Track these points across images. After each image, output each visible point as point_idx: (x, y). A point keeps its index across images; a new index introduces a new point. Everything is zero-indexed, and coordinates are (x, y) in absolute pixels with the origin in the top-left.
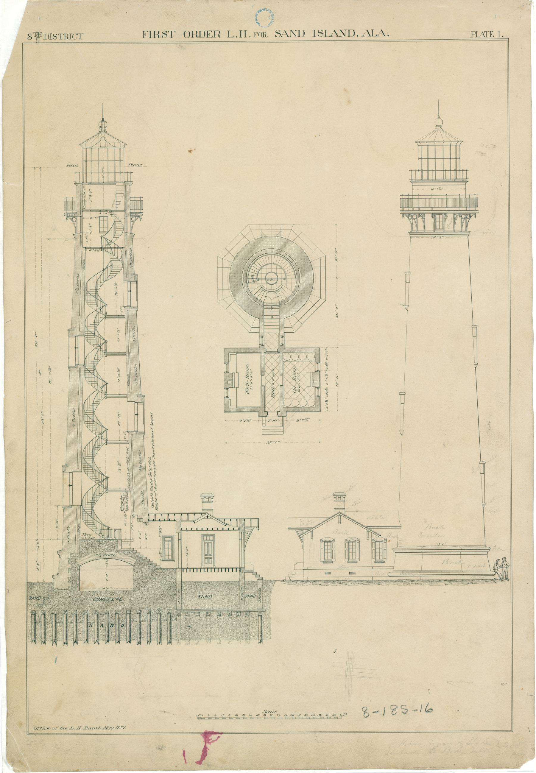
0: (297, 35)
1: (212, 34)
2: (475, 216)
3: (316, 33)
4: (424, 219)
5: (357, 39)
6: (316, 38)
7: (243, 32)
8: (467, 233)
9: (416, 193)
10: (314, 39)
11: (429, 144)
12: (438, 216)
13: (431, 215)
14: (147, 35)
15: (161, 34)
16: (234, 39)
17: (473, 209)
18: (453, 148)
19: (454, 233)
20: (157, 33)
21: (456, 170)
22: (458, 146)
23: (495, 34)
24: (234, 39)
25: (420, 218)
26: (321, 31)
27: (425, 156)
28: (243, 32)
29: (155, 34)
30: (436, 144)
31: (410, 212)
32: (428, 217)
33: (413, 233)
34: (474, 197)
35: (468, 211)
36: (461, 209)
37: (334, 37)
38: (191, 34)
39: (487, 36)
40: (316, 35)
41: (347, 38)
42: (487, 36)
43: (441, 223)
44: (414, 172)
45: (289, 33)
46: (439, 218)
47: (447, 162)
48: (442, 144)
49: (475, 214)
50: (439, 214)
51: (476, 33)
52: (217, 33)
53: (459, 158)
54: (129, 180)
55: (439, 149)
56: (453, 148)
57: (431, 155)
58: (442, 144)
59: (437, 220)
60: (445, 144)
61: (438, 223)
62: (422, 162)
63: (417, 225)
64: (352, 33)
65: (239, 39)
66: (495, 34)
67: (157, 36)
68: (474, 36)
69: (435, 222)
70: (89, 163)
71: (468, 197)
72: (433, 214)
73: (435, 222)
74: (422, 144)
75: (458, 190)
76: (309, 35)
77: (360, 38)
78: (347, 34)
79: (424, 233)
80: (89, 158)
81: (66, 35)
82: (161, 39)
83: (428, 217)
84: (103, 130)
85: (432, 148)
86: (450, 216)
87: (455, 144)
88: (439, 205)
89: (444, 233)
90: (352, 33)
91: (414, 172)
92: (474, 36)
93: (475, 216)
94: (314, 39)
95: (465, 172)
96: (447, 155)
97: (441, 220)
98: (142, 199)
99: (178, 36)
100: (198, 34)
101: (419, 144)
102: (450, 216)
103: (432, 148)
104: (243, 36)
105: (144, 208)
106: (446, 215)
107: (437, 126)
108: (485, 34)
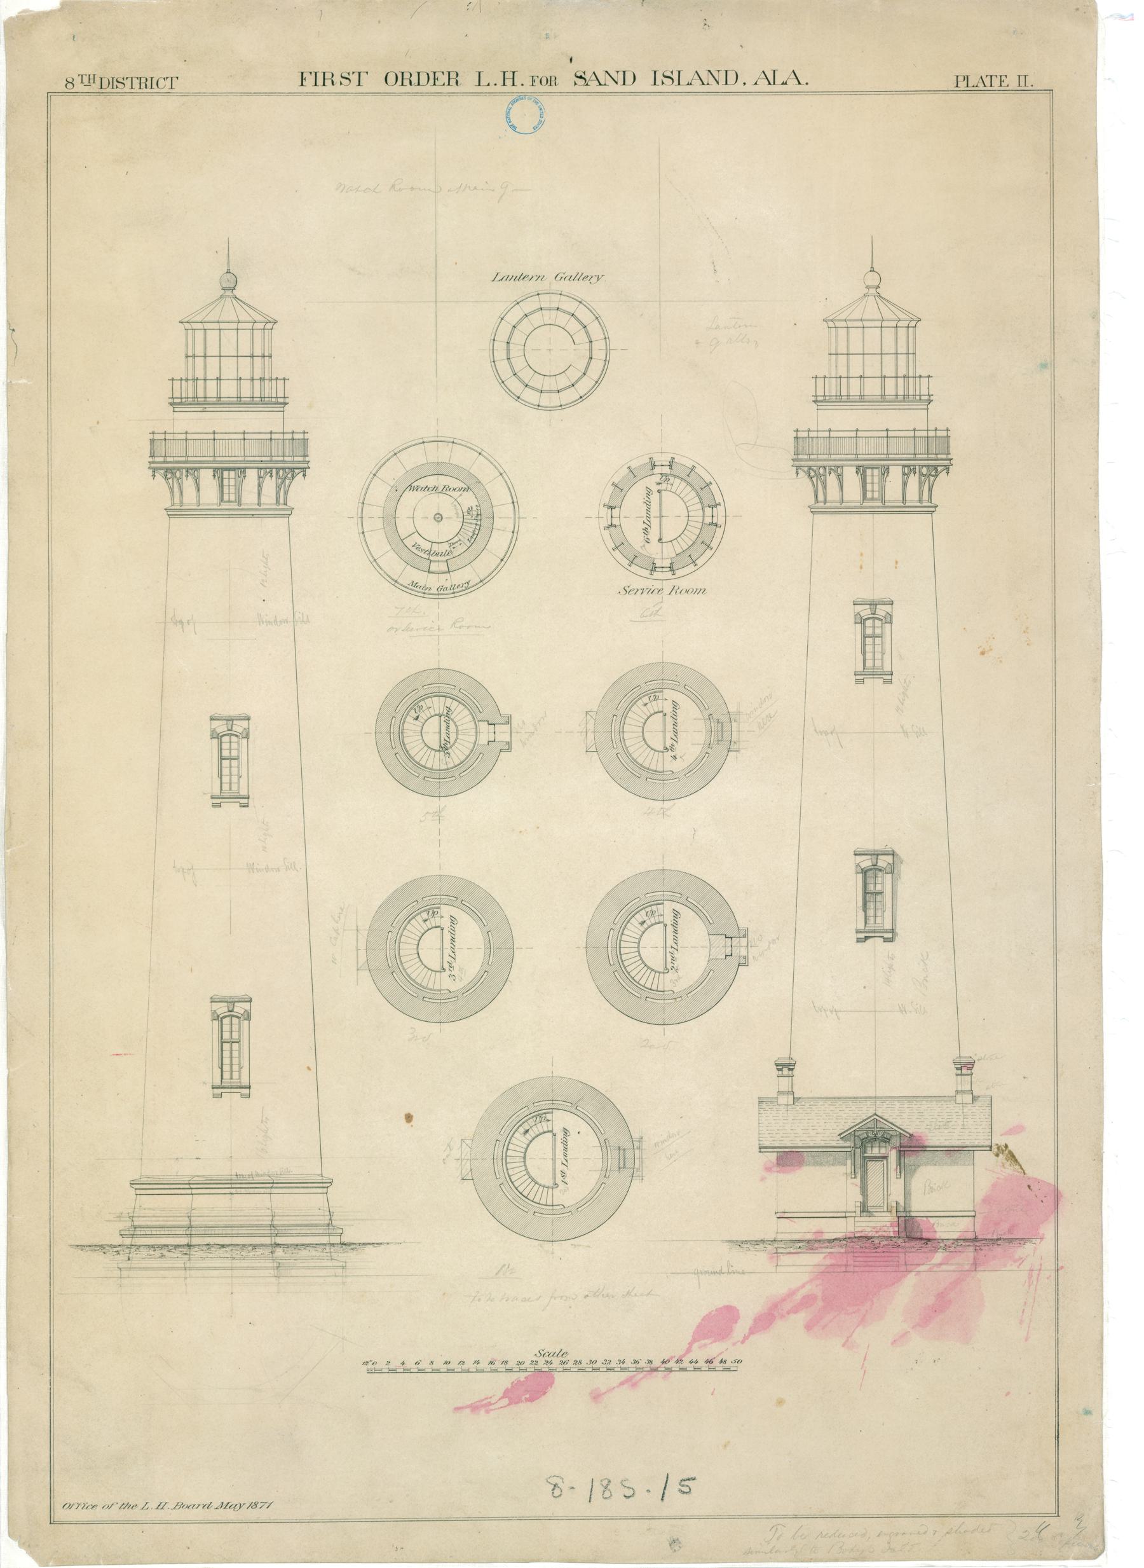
0: (621, 82)
2: (304, 475)
3: (659, 77)
4: (840, 477)
5: (744, 89)
6: (659, 88)
7: (509, 75)
8: (932, 510)
9: (180, 427)
10: (387, 89)
11: (207, 326)
12: (869, 472)
13: (854, 469)
14: (310, 80)
15: (337, 79)
16: (492, 89)
17: (301, 459)
18: (902, 332)
19: (903, 507)
20: (328, 76)
21: (262, 379)
22: (911, 330)
23: (1012, 82)
24: (492, 89)
25: (833, 474)
26: (669, 74)
27: (199, 351)
28: (509, 75)
29: (323, 78)
30: (223, 326)
31: (170, 467)
32: (850, 473)
33: (175, 512)
34: (301, 436)
35: (932, 462)
36: (296, 459)
37: (697, 86)
38: (400, 78)
39: (989, 84)
40: (659, 82)
41: (721, 87)
42: (989, 84)
43: (876, 487)
44: (177, 384)
46: (873, 476)
47: (889, 360)
48: (234, 326)
49: (304, 470)
50: (229, 469)
51: (966, 78)
52: (453, 75)
53: (271, 356)
54: (281, 394)
55: (855, 334)
56: (902, 332)
57: (213, 350)
58: (234, 326)
59: (869, 479)
60: (241, 326)
61: (869, 487)
62: (194, 363)
63: (930, 490)
65: (500, 88)
66: (1012, 82)
67: (328, 82)
68: (962, 85)
69: (221, 486)
70: (199, 361)
71: (932, 434)
72: (858, 468)
73: (221, 486)
74: (195, 326)
75: (259, 422)
76: (373, 82)
77: (749, 87)
78: (722, 81)
79: (200, 512)
80: (199, 351)
81: (143, 80)
82: (338, 88)
83: (850, 473)
84: (230, 288)
85: (213, 336)
86: (896, 473)
87: (261, 326)
88: (232, 451)
89: (240, 512)
90: (731, 78)
91: (177, 384)
92: (962, 85)
93: (304, 475)
94: (479, 89)
95: (281, 383)
96: (889, 347)
97: (876, 480)
98: (307, 436)
99: (373, 82)
100: (149, 83)
101: (188, 326)
102: (896, 473)
103: (213, 336)
104: (509, 82)
105: (952, 450)
106: (886, 470)
107: (868, 287)
108: (987, 81)
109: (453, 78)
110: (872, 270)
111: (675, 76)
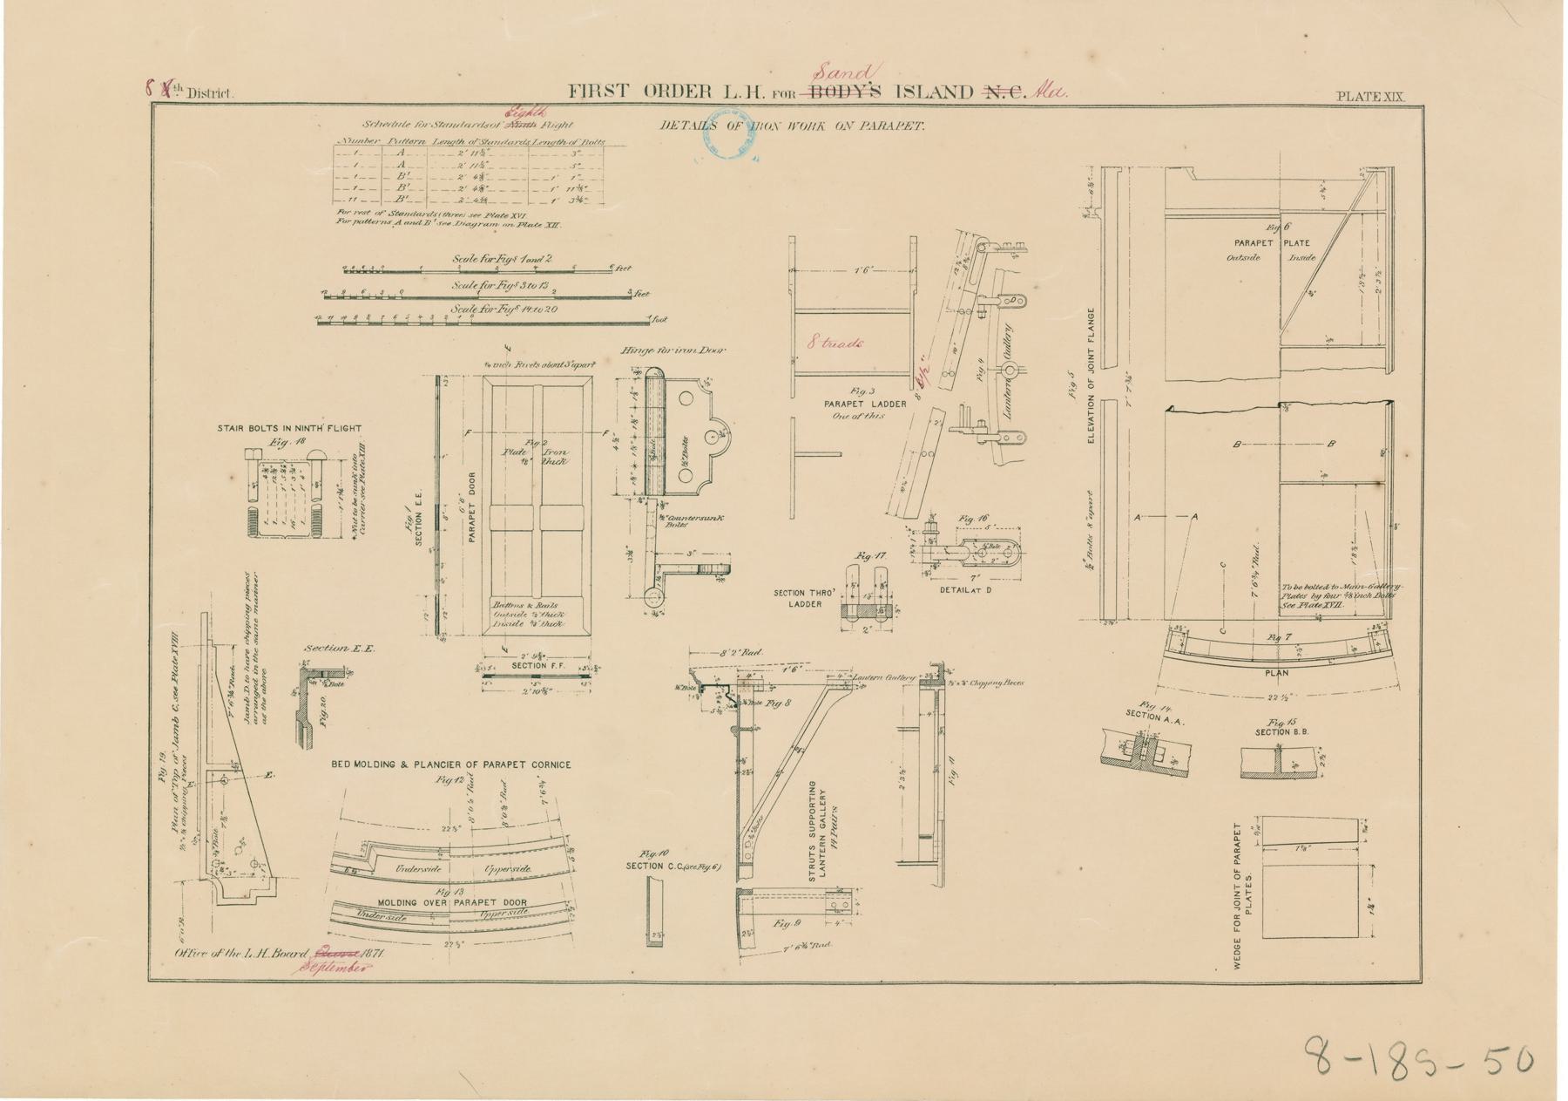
1: (697, 91)
3: (902, 92)
7: (753, 89)
14: (579, 91)
15: (603, 91)
28: (753, 89)
38: (659, 89)
42: (1394, 102)
45: (943, 92)
64: (967, 92)
78: (958, 95)
90: (967, 92)
104: (753, 95)
109: (705, 90)
110: (1008, 380)
111: (916, 91)
